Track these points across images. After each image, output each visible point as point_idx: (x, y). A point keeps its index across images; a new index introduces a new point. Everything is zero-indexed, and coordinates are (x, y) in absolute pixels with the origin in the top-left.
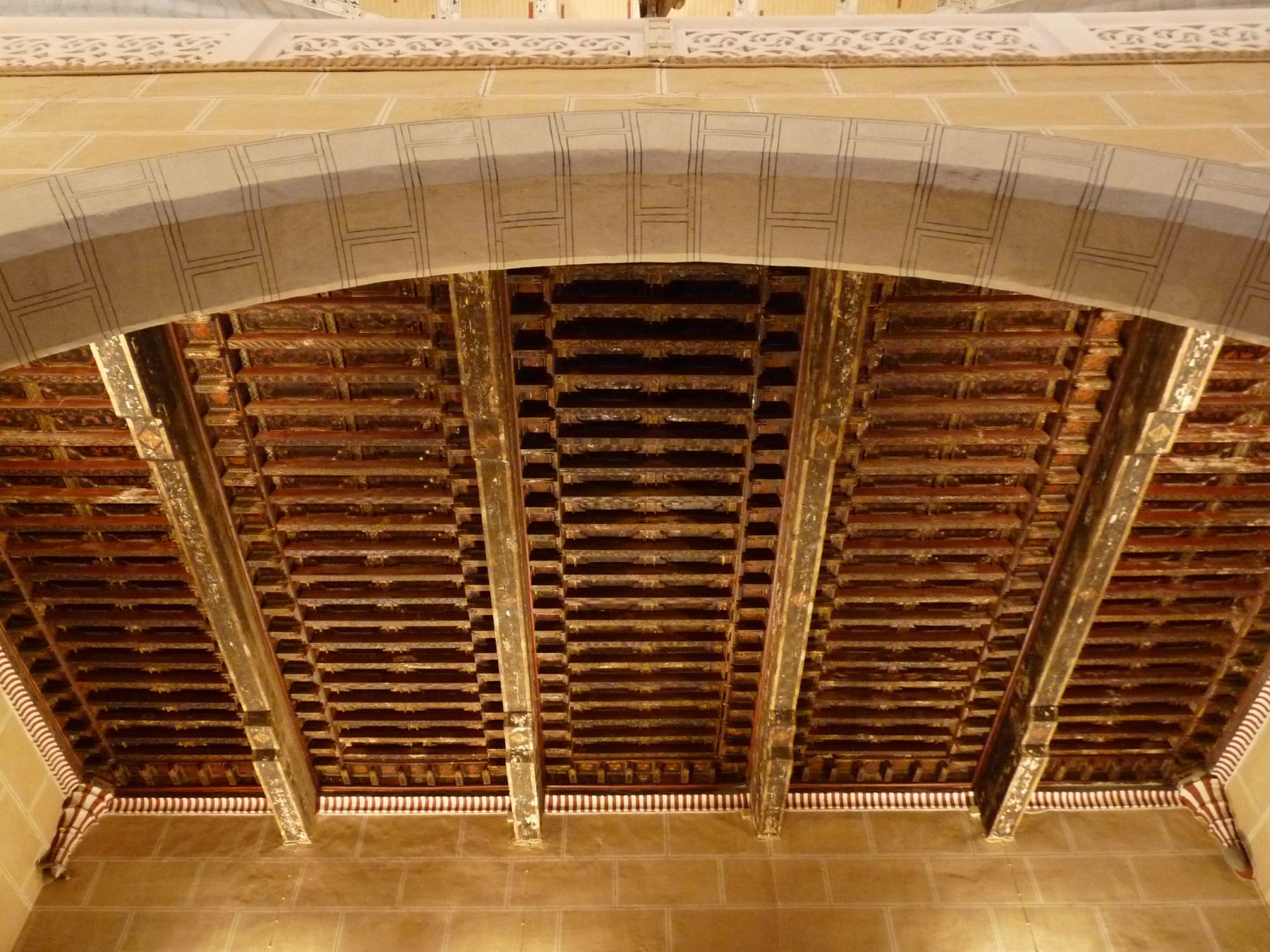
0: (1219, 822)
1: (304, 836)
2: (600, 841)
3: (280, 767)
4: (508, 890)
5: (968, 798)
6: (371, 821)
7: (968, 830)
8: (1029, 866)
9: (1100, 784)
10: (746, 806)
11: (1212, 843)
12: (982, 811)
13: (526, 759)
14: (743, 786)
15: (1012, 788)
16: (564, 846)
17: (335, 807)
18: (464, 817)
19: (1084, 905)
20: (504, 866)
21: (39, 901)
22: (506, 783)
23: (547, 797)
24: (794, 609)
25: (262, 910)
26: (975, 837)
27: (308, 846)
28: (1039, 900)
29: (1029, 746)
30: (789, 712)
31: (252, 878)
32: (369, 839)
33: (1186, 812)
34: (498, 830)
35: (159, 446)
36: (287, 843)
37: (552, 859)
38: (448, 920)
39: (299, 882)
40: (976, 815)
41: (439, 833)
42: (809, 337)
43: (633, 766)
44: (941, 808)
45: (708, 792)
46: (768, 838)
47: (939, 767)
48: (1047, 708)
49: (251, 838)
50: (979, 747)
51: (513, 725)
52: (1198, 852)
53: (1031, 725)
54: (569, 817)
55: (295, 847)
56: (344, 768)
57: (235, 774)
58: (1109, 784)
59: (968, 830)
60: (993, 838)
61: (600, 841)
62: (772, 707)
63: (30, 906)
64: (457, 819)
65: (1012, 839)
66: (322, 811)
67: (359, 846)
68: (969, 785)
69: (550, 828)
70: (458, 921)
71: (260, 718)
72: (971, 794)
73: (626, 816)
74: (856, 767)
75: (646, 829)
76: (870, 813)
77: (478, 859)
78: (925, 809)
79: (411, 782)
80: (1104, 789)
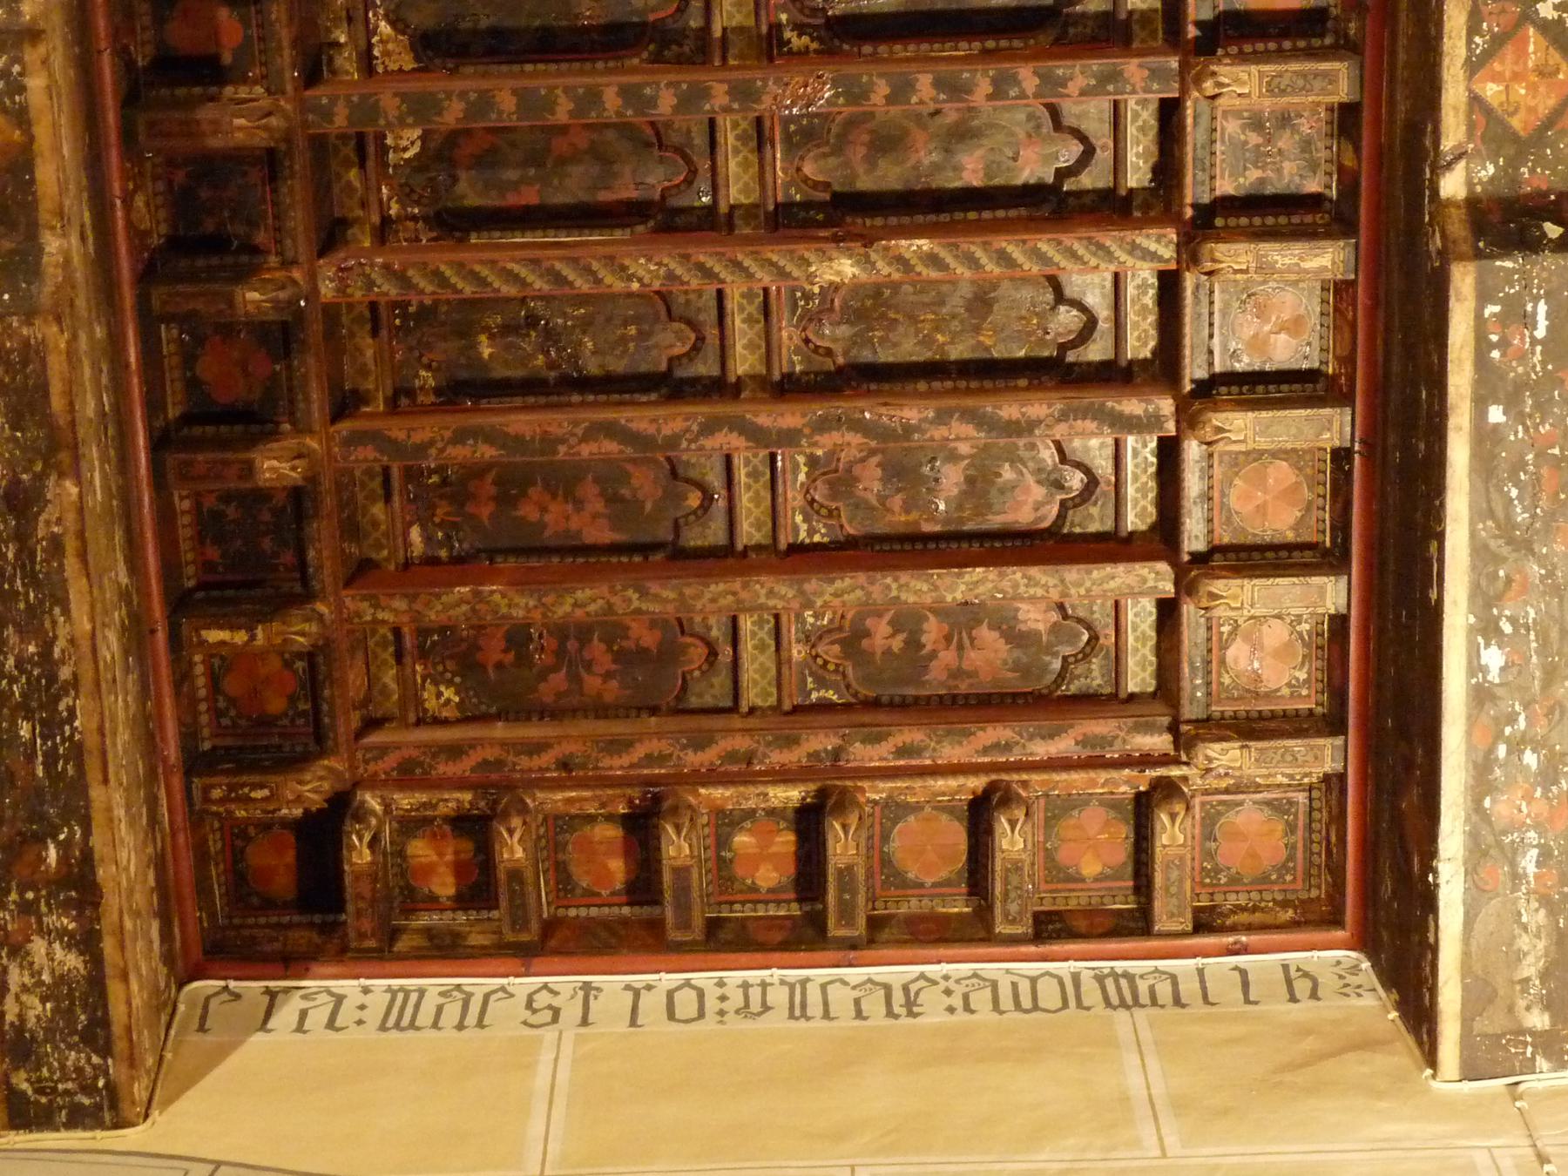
35: (1498, 42)
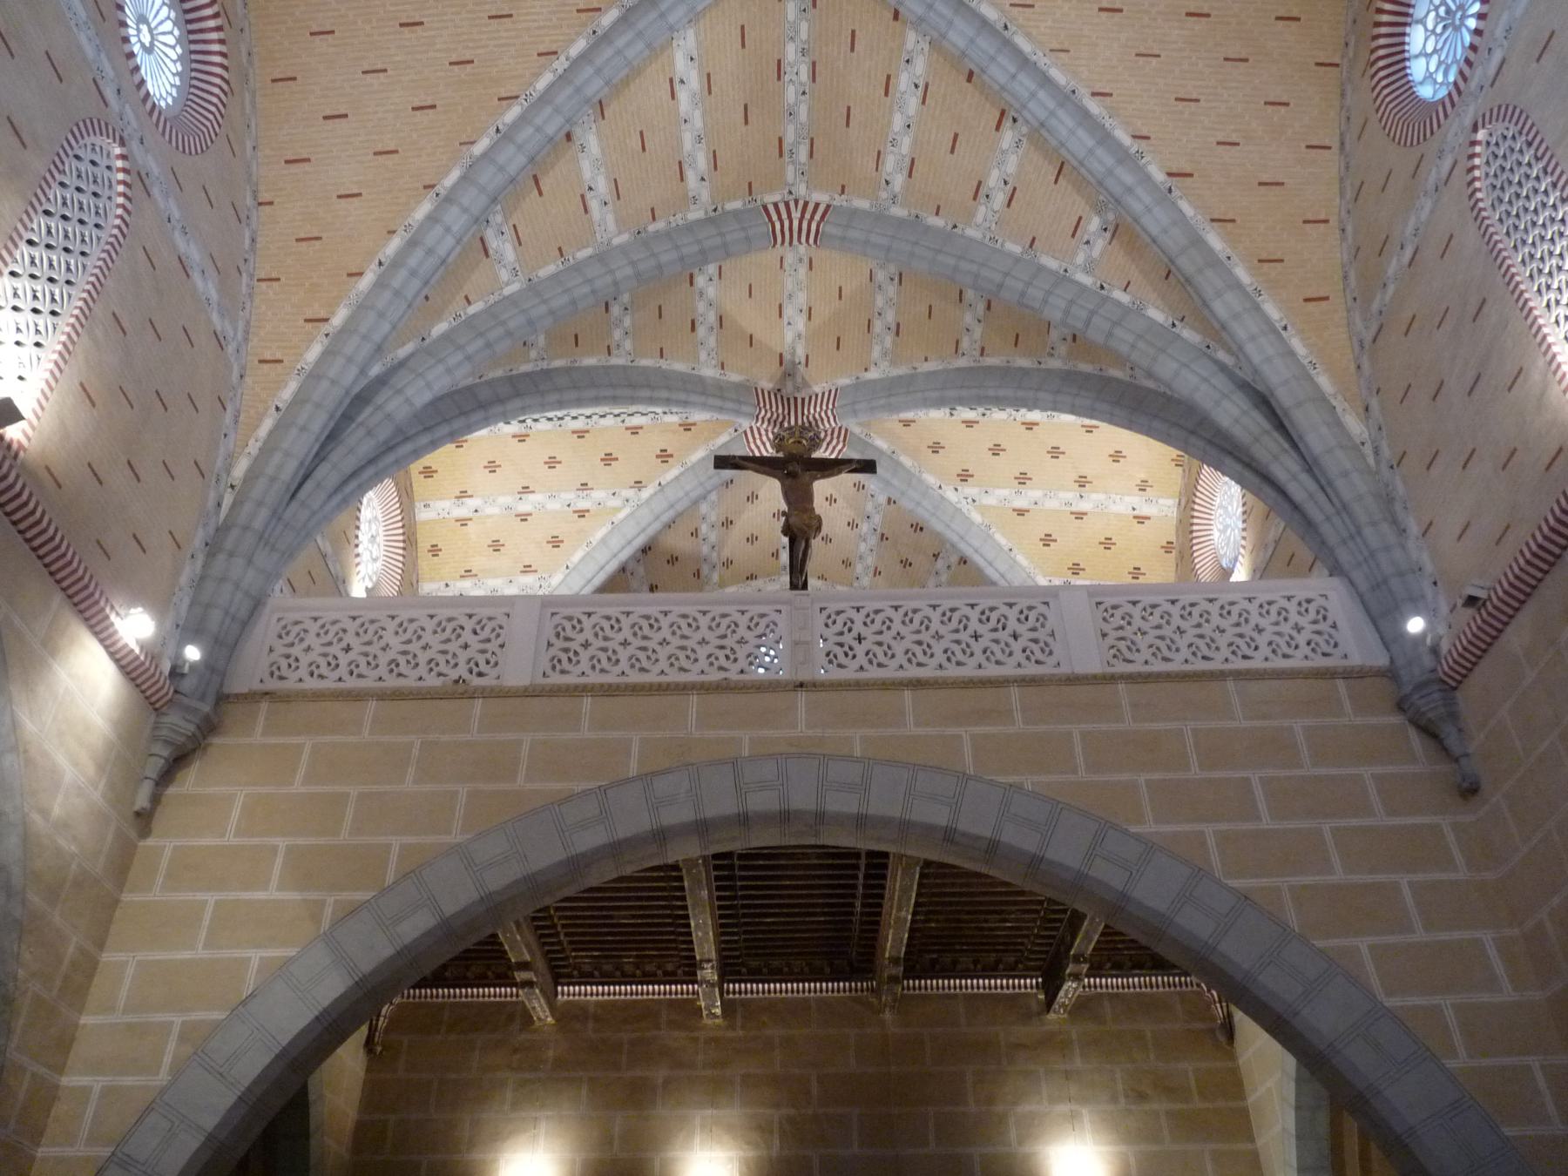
0: (1218, 1005)
1: (550, 1019)
2: (765, 1019)
3: (537, 991)
4: (700, 1057)
5: (1037, 983)
6: (598, 1003)
7: (1034, 1007)
8: (1074, 1037)
9: (1138, 972)
10: (873, 990)
11: (1213, 1019)
12: (1046, 994)
13: (713, 985)
14: (871, 975)
15: (1062, 993)
16: (739, 1024)
17: (569, 993)
18: (665, 1000)
19: (1108, 1066)
20: (696, 1040)
21: (369, 1070)
22: (691, 935)
23: (725, 985)
24: (898, 919)
25: (527, 1076)
26: (1039, 1014)
27: (554, 1025)
28: (1078, 1063)
29: (1070, 975)
30: (899, 958)
31: (516, 1051)
32: (597, 1019)
33: (1198, 993)
34: (688, 1011)
36: (537, 1024)
37: (730, 1034)
38: (660, 1081)
39: (551, 1053)
40: (1042, 997)
41: (644, 1013)
42: (887, 896)
43: (788, 965)
44: (1017, 990)
45: (844, 980)
46: (888, 1016)
47: (1017, 963)
48: (1083, 955)
49: (511, 1018)
50: (1048, 949)
51: (703, 968)
52: (1199, 1025)
53: (1070, 965)
54: (741, 1000)
55: (544, 1026)
56: (575, 969)
57: (493, 972)
58: (1144, 972)
59: (1034, 1007)
60: (1052, 1016)
61: (765, 1019)
62: (887, 955)
63: (362, 1074)
64: (659, 1001)
65: (1066, 1016)
66: (560, 997)
67: (590, 1025)
68: (1039, 973)
69: (728, 1007)
70: (667, 1082)
71: (524, 966)
72: (1040, 980)
73: (784, 998)
74: (955, 963)
75: (798, 1009)
76: (964, 995)
77: (676, 1034)
78: (1005, 991)
79: (624, 975)
80: (1139, 976)
